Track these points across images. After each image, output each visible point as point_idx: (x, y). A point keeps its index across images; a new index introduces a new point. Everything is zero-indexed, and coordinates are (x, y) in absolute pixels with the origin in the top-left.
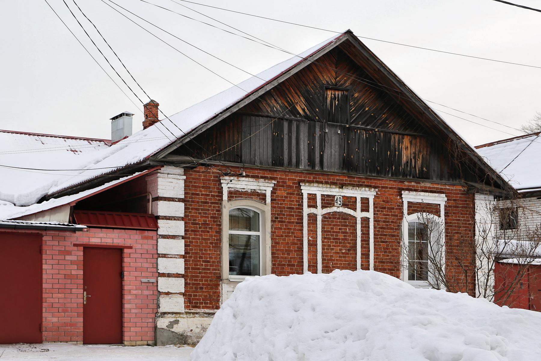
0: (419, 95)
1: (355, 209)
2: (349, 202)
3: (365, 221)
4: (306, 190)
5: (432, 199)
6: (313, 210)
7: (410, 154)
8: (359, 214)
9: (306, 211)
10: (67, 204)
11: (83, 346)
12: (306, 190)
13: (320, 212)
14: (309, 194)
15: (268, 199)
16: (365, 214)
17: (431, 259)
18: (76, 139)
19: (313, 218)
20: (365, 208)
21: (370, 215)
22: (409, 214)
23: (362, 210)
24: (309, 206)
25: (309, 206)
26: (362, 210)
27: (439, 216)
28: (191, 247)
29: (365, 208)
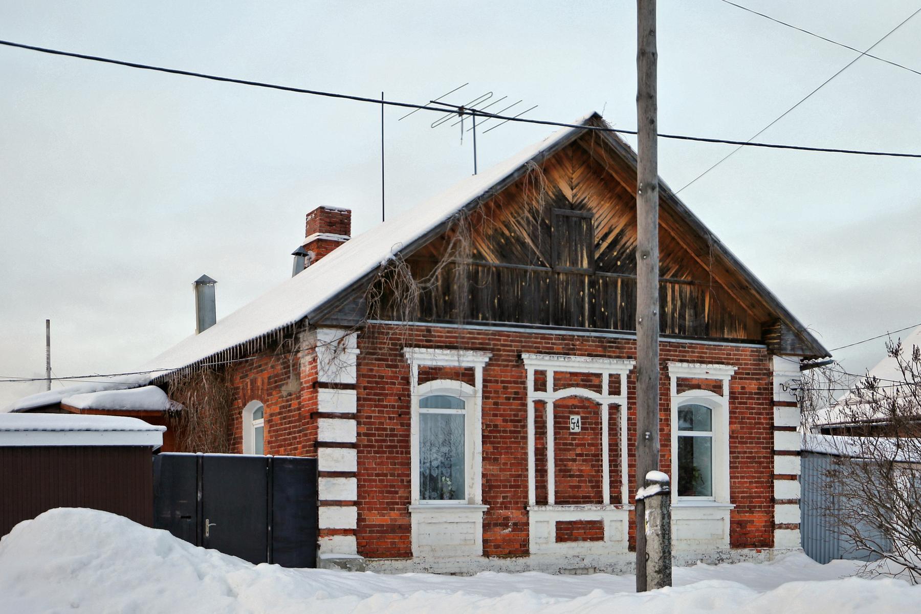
0: (533, 154)
1: (600, 392)
2: (590, 381)
3: (614, 408)
4: (532, 363)
5: (724, 374)
6: (540, 395)
7: (337, 319)
8: (605, 399)
9: (533, 395)
10: (789, 475)
11: (567, 601)
12: (532, 363)
13: (551, 396)
14: (536, 372)
15: (726, 390)
16: (615, 399)
17: (858, 479)
18: (48, 344)
19: (540, 405)
20: (615, 390)
21: (622, 400)
22: (678, 392)
23: (610, 393)
24: (536, 389)
25: (536, 389)
26: (610, 393)
27: (473, 384)
28: (493, 457)
29: (615, 390)
